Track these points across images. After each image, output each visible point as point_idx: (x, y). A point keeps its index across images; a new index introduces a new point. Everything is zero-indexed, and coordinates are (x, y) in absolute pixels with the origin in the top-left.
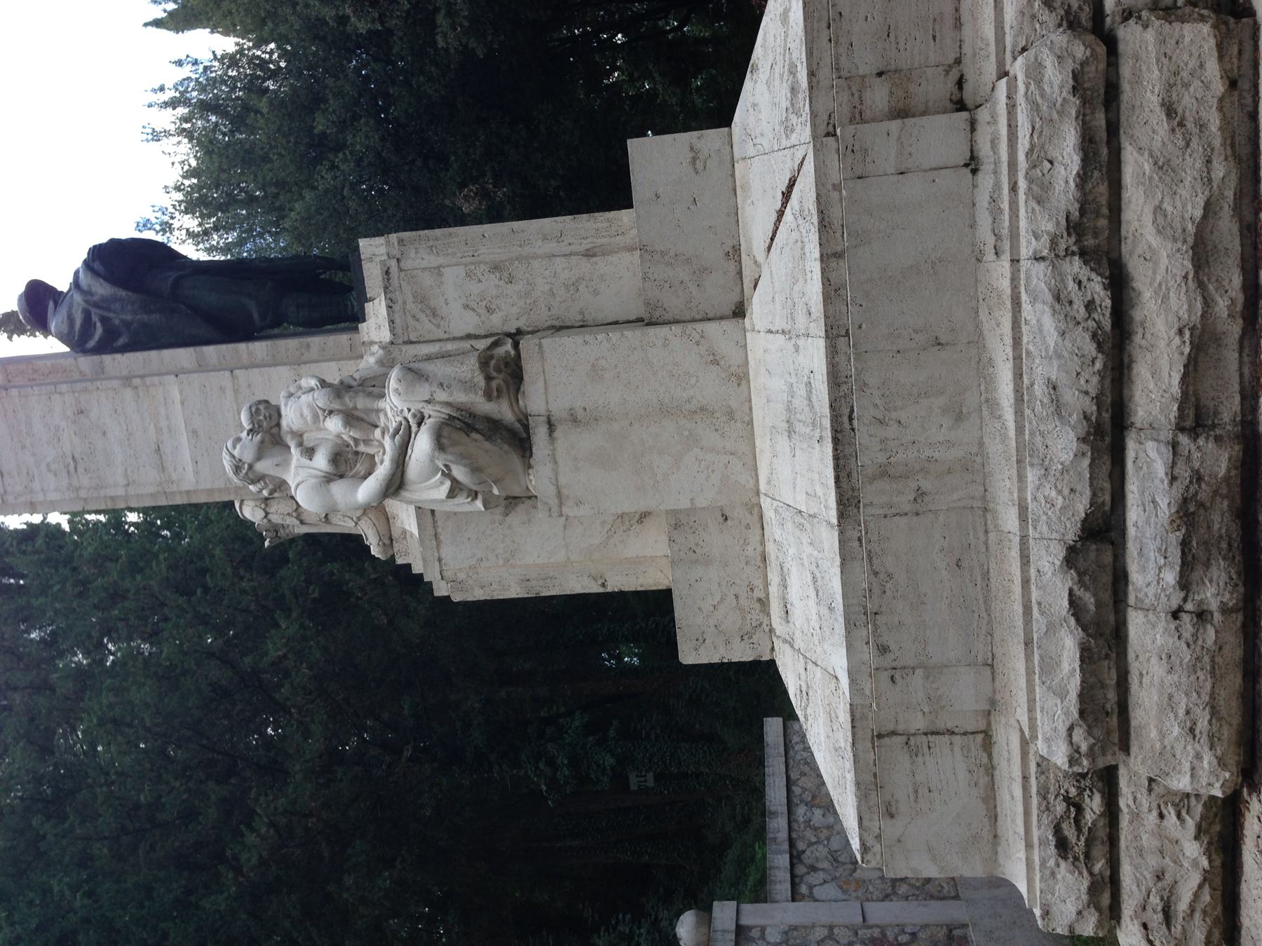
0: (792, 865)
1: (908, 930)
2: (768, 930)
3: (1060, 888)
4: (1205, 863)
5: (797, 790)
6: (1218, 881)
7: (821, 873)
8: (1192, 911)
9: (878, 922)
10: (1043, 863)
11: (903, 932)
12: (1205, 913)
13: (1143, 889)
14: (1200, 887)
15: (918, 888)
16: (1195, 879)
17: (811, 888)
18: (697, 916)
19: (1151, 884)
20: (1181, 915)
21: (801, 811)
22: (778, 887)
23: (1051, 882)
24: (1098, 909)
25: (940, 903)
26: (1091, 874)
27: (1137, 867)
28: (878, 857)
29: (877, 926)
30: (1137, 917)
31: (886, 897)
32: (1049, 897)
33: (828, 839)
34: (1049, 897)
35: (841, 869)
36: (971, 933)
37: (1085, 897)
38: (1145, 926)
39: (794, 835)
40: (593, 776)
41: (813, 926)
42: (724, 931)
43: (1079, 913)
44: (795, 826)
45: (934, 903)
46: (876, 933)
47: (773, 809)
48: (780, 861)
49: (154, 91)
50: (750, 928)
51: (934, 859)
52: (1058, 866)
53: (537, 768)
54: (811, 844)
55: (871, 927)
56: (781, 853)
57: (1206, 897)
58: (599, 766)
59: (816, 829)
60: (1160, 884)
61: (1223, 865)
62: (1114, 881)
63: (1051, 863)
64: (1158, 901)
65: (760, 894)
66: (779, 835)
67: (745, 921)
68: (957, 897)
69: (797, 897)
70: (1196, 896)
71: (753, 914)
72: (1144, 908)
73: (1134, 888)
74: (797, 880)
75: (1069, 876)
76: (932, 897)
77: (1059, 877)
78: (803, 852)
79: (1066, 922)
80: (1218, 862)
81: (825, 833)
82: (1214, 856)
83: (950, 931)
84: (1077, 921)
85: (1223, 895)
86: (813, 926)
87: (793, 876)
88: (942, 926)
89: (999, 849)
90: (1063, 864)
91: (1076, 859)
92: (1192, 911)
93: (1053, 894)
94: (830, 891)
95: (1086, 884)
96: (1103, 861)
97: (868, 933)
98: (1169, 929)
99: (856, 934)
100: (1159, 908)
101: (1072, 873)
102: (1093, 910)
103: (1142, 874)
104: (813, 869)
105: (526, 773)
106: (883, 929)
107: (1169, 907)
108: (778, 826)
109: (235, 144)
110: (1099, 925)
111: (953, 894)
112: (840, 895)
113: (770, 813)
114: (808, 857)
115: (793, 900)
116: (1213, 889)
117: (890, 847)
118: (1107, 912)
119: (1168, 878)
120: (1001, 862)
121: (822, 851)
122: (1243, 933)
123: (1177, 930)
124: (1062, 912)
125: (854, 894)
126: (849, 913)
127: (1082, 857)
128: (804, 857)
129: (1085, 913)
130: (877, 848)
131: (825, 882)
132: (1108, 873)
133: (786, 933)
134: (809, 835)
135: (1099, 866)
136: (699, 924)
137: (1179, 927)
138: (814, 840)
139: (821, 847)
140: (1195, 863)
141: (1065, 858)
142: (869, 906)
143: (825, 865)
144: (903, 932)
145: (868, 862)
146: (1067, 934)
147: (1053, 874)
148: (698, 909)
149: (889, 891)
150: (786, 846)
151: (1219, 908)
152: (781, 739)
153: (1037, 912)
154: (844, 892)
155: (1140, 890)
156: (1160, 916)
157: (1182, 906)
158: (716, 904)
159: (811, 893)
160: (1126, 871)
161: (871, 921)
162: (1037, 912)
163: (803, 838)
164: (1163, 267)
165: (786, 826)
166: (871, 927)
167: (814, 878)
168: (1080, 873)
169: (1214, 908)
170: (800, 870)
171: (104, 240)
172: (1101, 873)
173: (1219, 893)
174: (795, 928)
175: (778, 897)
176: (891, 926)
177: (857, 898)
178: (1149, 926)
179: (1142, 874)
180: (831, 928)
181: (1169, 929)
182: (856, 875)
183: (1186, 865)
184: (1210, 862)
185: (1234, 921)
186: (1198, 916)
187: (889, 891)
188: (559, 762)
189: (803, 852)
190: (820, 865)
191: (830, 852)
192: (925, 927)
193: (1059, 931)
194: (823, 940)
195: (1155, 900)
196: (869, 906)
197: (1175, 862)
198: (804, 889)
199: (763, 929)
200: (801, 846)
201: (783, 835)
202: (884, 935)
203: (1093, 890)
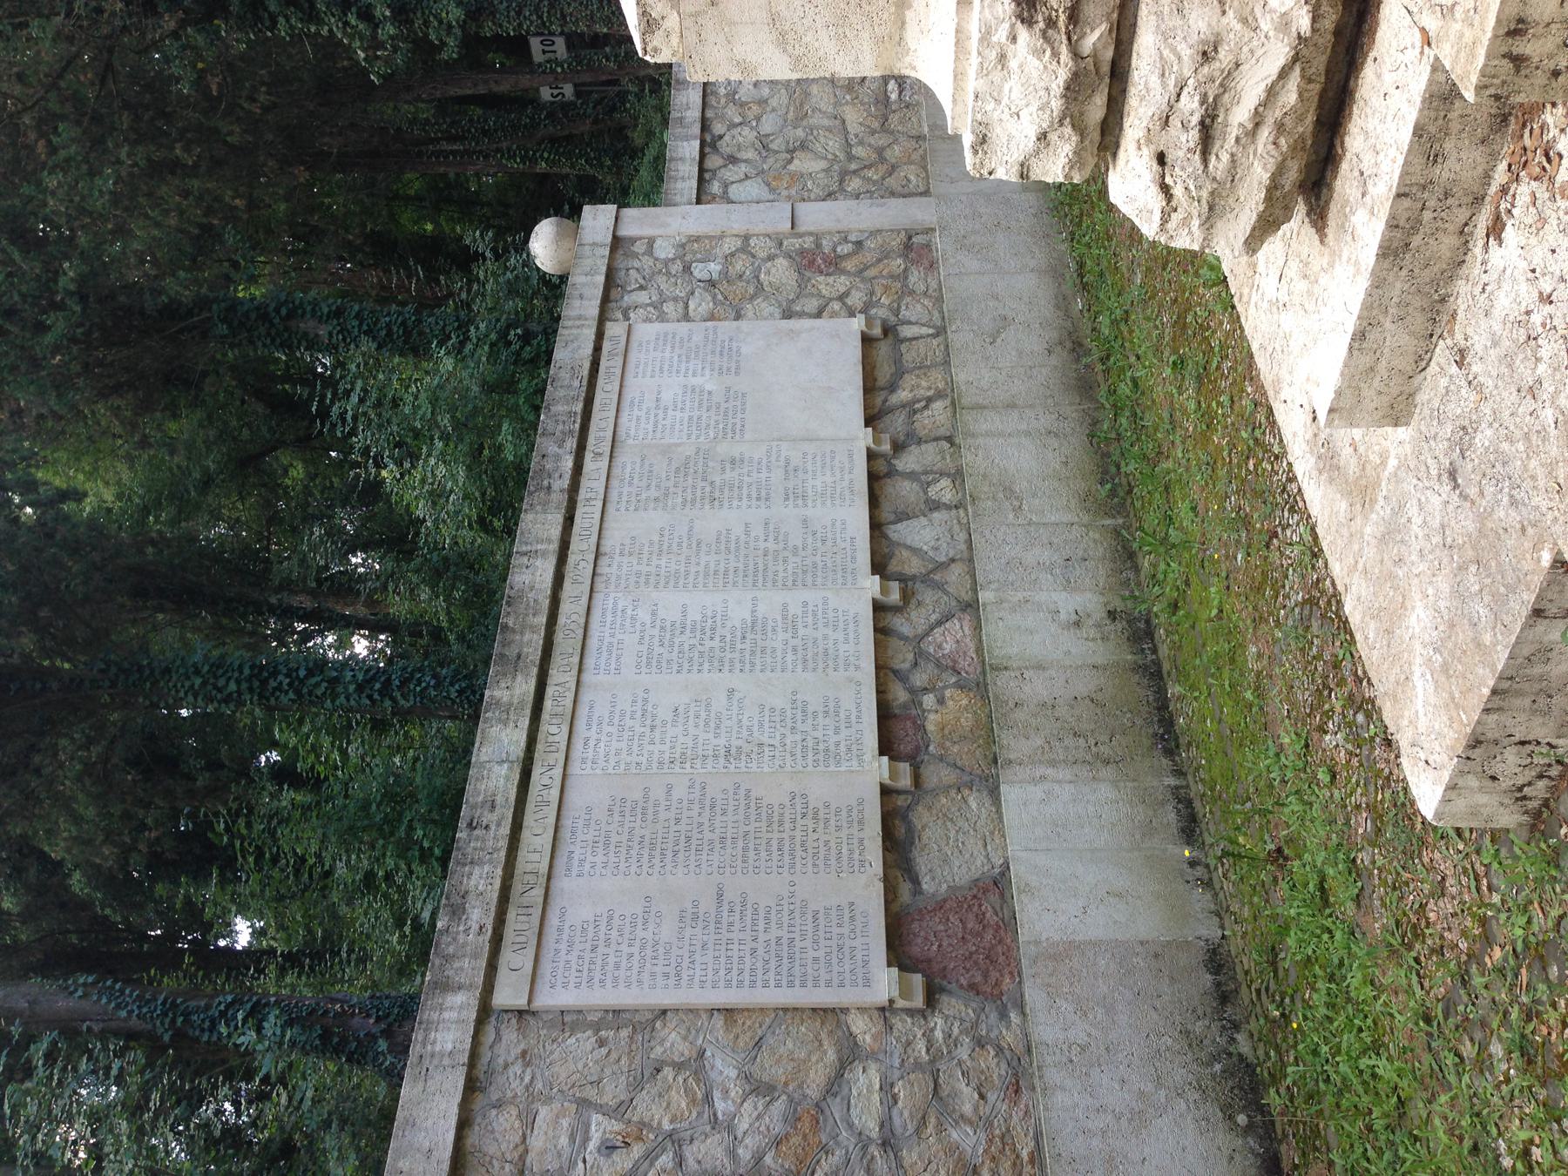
0: (702, 155)
1: (853, 238)
2: (658, 242)
3: (1013, 89)
4: (1303, 22)
6: (1320, 63)
7: (743, 165)
8: (1257, 125)
9: (812, 229)
10: (985, 38)
11: (846, 240)
12: (1280, 127)
13: (1171, 82)
14: (1283, 74)
15: (875, 183)
16: (1278, 54)
17: (726, 186)
18: (558, 225)
19: (1187, 72)
20: (1234, 132)
22: (679, 185)
23: (997, 76)
24: (1080, 129)
25: (901, 200)
26: (1076, 55)
27: (1166, 36)
28: (675, 40)
29: (811, 234)
30: (1149, 141)
31: (830, 196)
32: (990, 106)
33: (758, 119)
34: (990, 106)
35: (771, 160)
36: (937, 240)
37: (1057, 104)
38: (1161, 159)
39: (709, 114)
40: (433, 37)
41: (722, 237)
42: (594, 244)
43: (1043, 137)
44: (712, 100)
45: (893, 202)
46: (808, 243)
48: (684, 150)
50: (633, 240)
51: (782, 41)
52: (1014, 39)
53: (346, 24)
54: (733, 126)
55: (801, 236)
56: (687, 138)
57: (1290, 96)
58: (441, 22)
59: (742, 105)
60: (1206, 70)
61: (1337, 33)
62: (1119, 73)
63: (1001, 35)
64: (1196, 105)
65: (652, 195)
66: (689, 113)
67: (624, 232)
68: (926, 193)
69: (704, 198)
70: (1272, 93)
71: (637, 222)
72: (1166, 122)
73: (1155, 81)
74: (707, 176)
75: (1034, 64)
76: (893, 194)
77: (1013, 64)
78: (721, 137)
79: (1016, 156)
80: (1328, 23)
82: (1325, 8)
83: (910, 238)
84: (1037, 152)
85: (1322, 95)
86: (722, 237)
87: (702, 170)
88: (899, 232)
89: (909, 15)
90: (1023, 34)
91: (1051, 23)
92: (1257, 125)
93: (998, 101)
94: (754, 189)
95: (1063, 75)
96: (1104, 27)
97: (796, 243)
98: (1205, 162)
99: (781, 244)
100: (1195, 119)
101: (1038, 53)
102: (1068, 130)
103: (1174, 50)
104: (732, 160)
105: (331, 31)
106: (818, 237)
107: (1214, 118)
110: (1077, 160)
111: (922, 189)
112: (765, 194)
113: (678, 81)
114: (725, 146)
115: (699, 202)
116: (1307, 79)
117: (697, 14)
118: (1096, 136)
119: (1224, 57)
120: (912, 45)
121: (748, 134)
122: (1344, 166)
123: (1220, 163)
124: (1010, 137)
125: (785, 193)
126: (776, 218)
127: (1063, 18)
128: (722, 144)
129: (1053, 137)
130: (672, 22)
131: (747, 177)
132: (1109, 54)
133: (683, 246)
134: (733, 114)
135: (1094, 37)
136: (560, 236)
137: (1225, 157)
138: (737, 120)
139: (746, 131)
140: (1285, 22)
141: (1029, 22)
142: (802, 208)
143: (750, 154)
144: (846, 240)
145: (656, 50)
146: (1014, 179)
147: (1002, 58)
148: (558, 213)
149: (835, 187)
150: (696, 129)
151: (1310, 118)
153: (968, 140)
154: (772, 190)
155: (1164, 85)
156: (1194, 135)
157: (1240, 115)
158: (586, 208)
159: (726, 192)
160: (1146, 43)
161: (802, 229)
162: (968, 140)
163: (722, 117)
165: (699, 101)
166: (801, 236)
167: (731, 173)
168: (1056, 55)
169: (1300, 119)
170: (713, 161)
172: (1095, 55)
173: (1316, 88)
174: (697, 239)
175: (678, 198)
176: (830, 233)
177: (789, 197)
178: (1168, 160)
179: (1174, 50)
180: (746, 238)
181: (1205, 162)
182: (791, 167)
183: (1266, 25)
184: (1314, 20)
185: (1331, 146)
186: (1265, 133)
187: (835, 187)
188: (378, 13)
189: (721, 137)
190: (743, 155)
191: (760, 137)
192: (874, 233)
193: (1001, 174)
194: (732, 255)
195: (1190, 105)
196: (802, 208)
197: (1244, 21)
198: (715, 187)
199: (651, 241)
200: (718, 128)
201: (694, 114)
202: (818, 245)
203: (1075, 90)
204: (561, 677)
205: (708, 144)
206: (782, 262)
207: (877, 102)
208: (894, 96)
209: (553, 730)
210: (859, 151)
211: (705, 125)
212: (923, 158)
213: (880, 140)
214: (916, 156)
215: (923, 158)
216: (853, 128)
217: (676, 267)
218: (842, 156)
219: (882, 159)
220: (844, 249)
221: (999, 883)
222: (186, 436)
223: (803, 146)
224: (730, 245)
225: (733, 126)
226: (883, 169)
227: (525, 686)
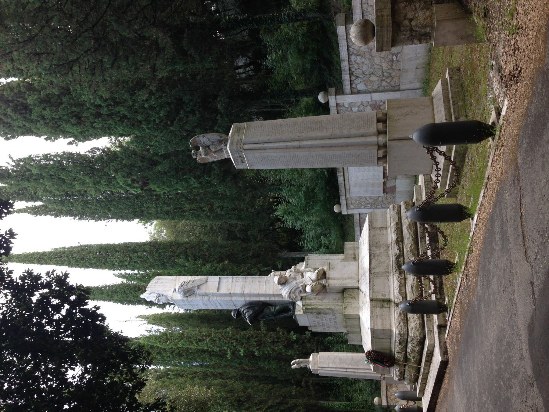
0: (350, 77)
5: (351, 50)
17: (356, 85)
21: (353, 57)
44: (351, 63)
47: (343, 59)
49: (147, 331)
54: (356, 69)
56: (346, 74)
65: (340, 91)
81: (361, 65)
87: (351, 81)
97: (372, 102)
108: (345, 65)
109: (31, 76)
134: (356, 66)
138: (357, 68)
150: (348, 72)
152: (345, 33)
164: (480, 202)
171: (112, 243)
200: (353, 70)
201: (347, 68)
204: (346, 174)
205: (351, 74)
206: (369, 107)
207: (390, 61)
208: (395, 59)
209: (346, 178)
210: (385, 74)
211: (350, 69)
212: (400, 76)
213: (390, 71)
214: (398, 75)
215: (400, 76)
216: (384, 68)
217: (349, 109)
218: (381, 76)
219: (390, 76)
220: (381, 103)
221: (395, 186)
222: (56, 47)
223: (373, 73)
224: (359, 104)
225: (356, 69)
226: (390, 78)
227: (342, 174)
